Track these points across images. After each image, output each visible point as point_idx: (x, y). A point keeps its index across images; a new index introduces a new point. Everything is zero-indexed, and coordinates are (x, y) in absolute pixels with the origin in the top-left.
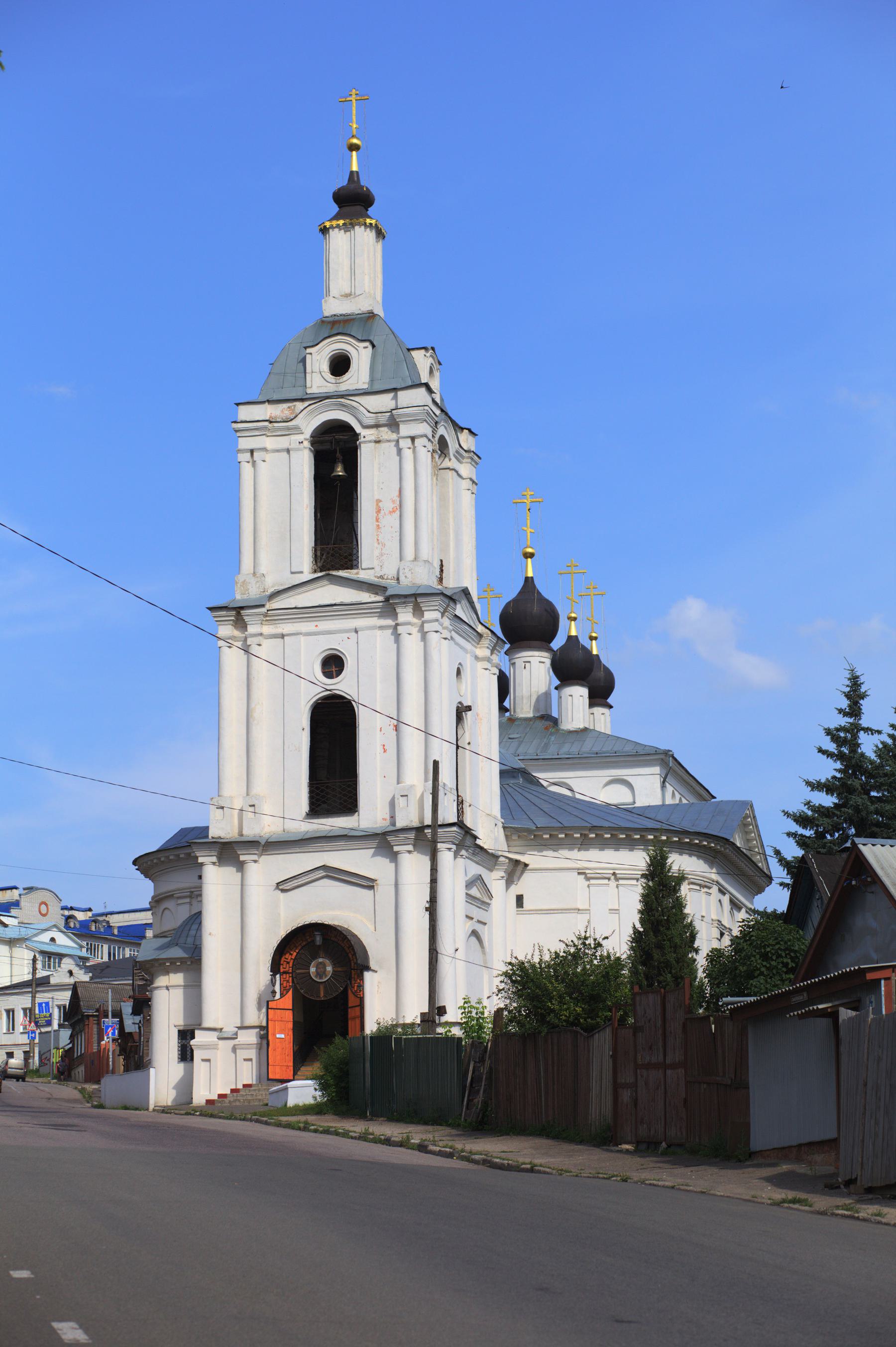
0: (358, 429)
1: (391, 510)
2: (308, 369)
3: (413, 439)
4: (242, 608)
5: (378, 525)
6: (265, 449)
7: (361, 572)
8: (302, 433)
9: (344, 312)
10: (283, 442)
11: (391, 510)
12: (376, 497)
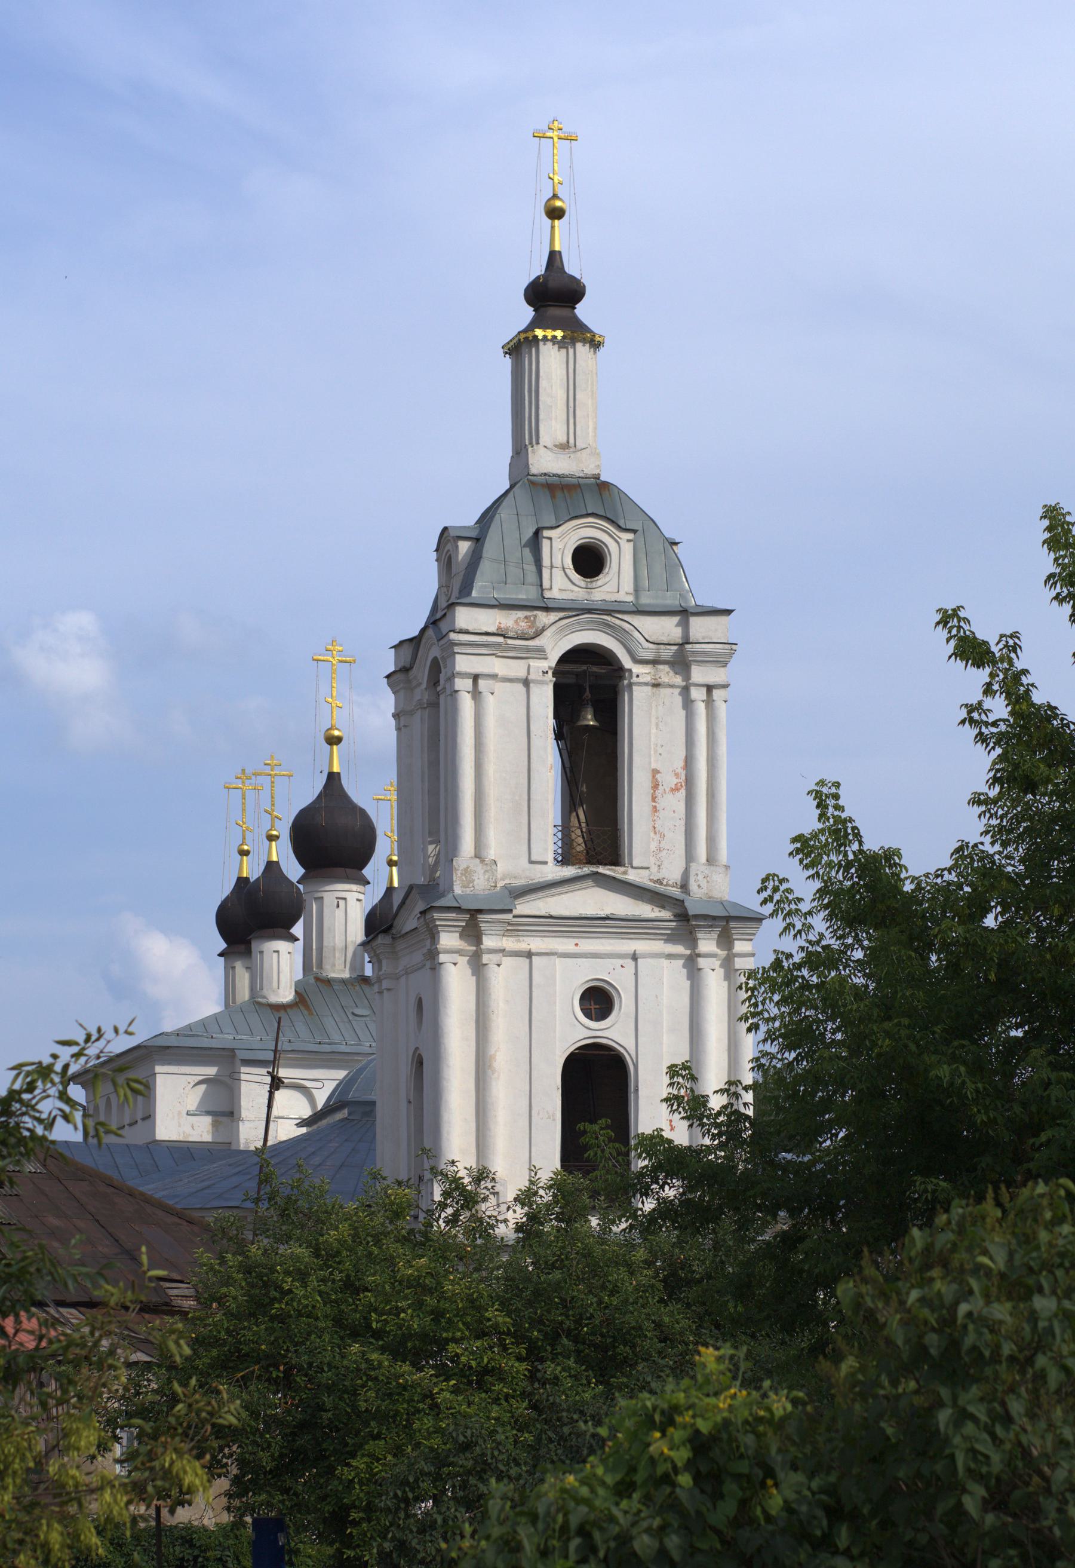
0: (627, 662)
1: (673, 787)
2: (546, 561)
3: (710, 688)
4: (480, 911)
5: (655, 807)
6: (494, 677)
7: (630, 871)
8: (546, 659)
9: (560, 472)
10: (517, 668)
11: (673, 787)
12: (654, 766)
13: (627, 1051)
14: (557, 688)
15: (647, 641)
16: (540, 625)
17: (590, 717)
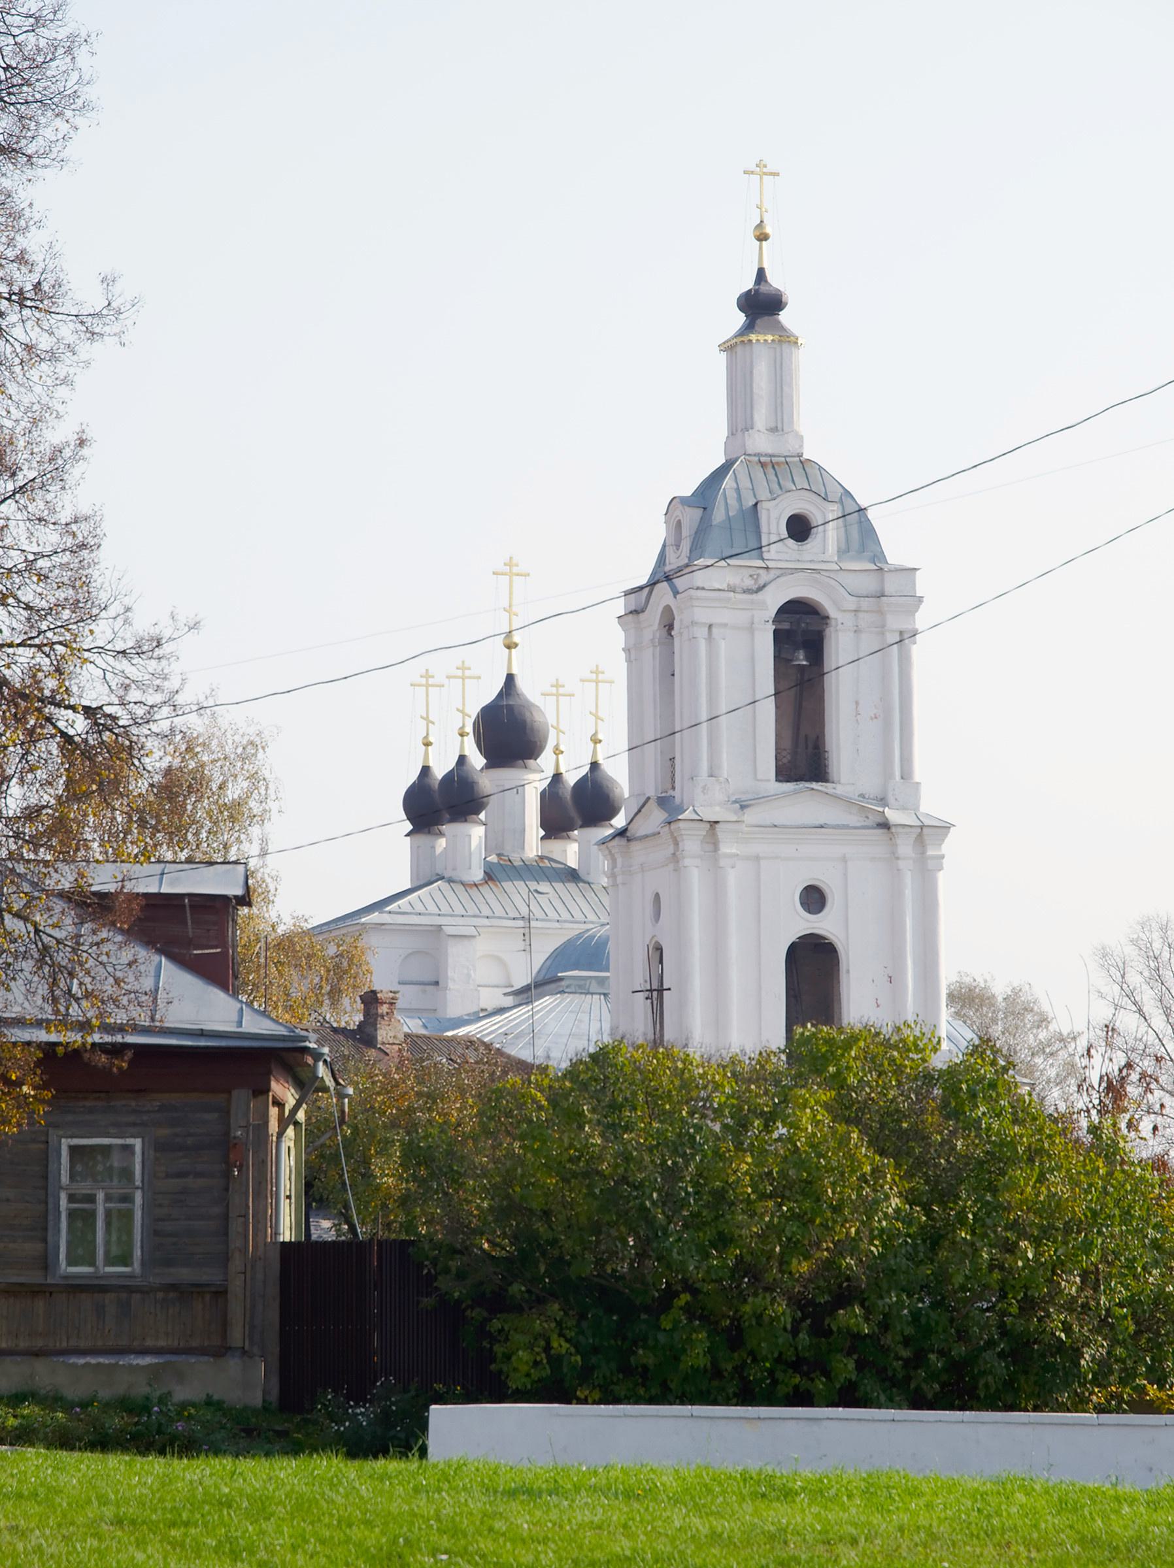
4: (717, 822)
14: (777, 634)
16: (761, 582)
17: (801, 657)
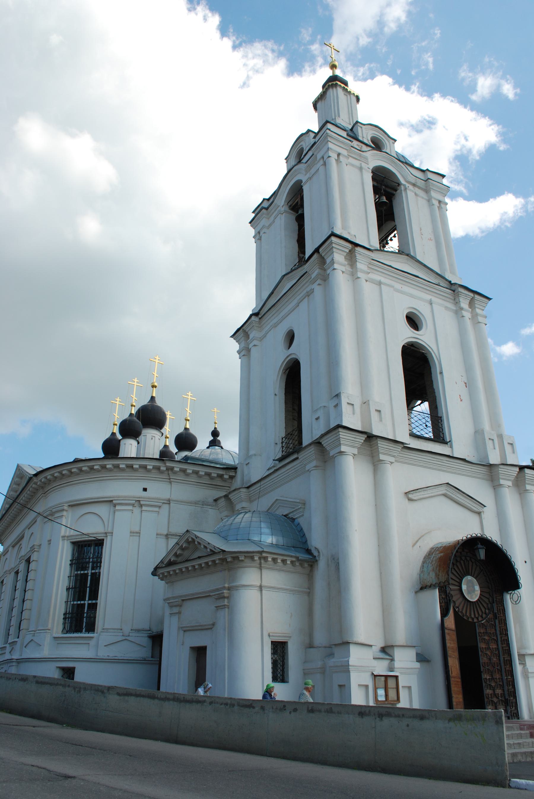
13: (433, 351)
15: (412, 174)
